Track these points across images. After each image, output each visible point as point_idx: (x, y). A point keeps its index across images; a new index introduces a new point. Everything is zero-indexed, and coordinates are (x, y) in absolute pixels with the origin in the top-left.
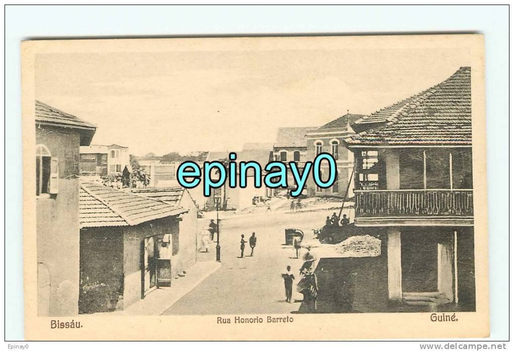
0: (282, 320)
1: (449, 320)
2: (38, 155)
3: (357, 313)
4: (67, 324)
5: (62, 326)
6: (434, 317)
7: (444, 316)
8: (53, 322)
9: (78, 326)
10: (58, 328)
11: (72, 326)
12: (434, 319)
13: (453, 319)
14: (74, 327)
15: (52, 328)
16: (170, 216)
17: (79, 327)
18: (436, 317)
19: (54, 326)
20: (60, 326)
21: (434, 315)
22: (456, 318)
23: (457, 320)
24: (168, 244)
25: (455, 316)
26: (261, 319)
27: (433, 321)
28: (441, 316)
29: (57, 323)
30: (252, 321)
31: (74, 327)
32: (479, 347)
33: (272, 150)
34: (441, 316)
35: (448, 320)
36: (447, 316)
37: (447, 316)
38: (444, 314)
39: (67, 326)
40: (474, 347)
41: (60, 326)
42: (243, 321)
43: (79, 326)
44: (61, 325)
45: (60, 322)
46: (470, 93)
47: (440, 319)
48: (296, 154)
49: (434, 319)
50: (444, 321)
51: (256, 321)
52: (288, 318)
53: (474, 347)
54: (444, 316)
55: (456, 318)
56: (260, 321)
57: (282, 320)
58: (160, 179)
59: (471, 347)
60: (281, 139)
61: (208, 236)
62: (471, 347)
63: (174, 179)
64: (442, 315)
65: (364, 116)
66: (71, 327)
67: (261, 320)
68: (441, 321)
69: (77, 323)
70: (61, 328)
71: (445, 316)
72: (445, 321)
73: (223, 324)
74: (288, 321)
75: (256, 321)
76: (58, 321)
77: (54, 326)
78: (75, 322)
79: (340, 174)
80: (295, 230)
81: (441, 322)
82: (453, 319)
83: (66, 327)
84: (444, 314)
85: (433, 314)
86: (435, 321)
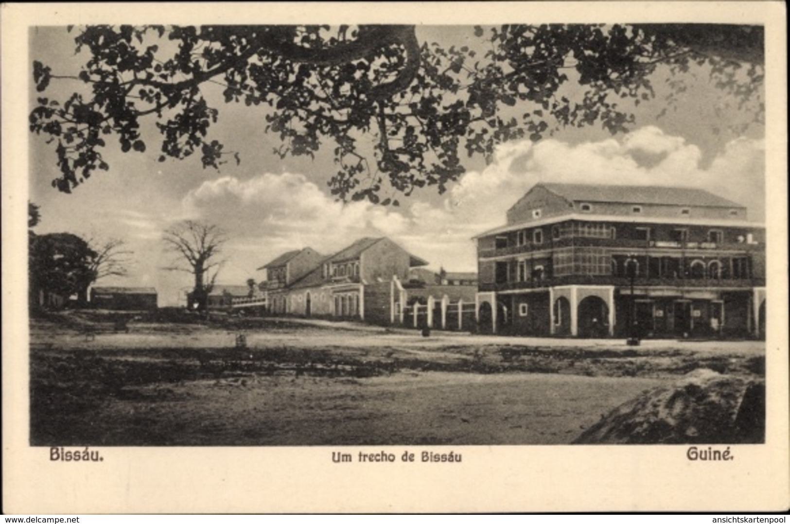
0: (367, 459)
2: (49, 101)
5: (69, 458)
7: (710, 453)
9: (94, 457)
11: (86, 458)
15: (52, 459)
17: (97, 460)
18: (696, 453)
24: (175, 414)
25: (728, 452)
28: (706, 452)
30: (444, 458)
31: (88, 459)
37: (715, 452)
38: (710, 448)
39: (77, 458)
41: (65, 457)
47: (703, 456)
49: (693, 456)
50: (710, 459)
54: (710, 453)
55: (730, 455)
56: (391, 458)
57: (367, 459)
58: (179, 310)
60: (413, 106)
64: (708, 450)
65: (187, 257)
66: (84, 459)
67: (391, 458)
70: (67, 460)
71: (712, 450)
79: (420, 276)
82: (726, 456)
84: (710, 448)
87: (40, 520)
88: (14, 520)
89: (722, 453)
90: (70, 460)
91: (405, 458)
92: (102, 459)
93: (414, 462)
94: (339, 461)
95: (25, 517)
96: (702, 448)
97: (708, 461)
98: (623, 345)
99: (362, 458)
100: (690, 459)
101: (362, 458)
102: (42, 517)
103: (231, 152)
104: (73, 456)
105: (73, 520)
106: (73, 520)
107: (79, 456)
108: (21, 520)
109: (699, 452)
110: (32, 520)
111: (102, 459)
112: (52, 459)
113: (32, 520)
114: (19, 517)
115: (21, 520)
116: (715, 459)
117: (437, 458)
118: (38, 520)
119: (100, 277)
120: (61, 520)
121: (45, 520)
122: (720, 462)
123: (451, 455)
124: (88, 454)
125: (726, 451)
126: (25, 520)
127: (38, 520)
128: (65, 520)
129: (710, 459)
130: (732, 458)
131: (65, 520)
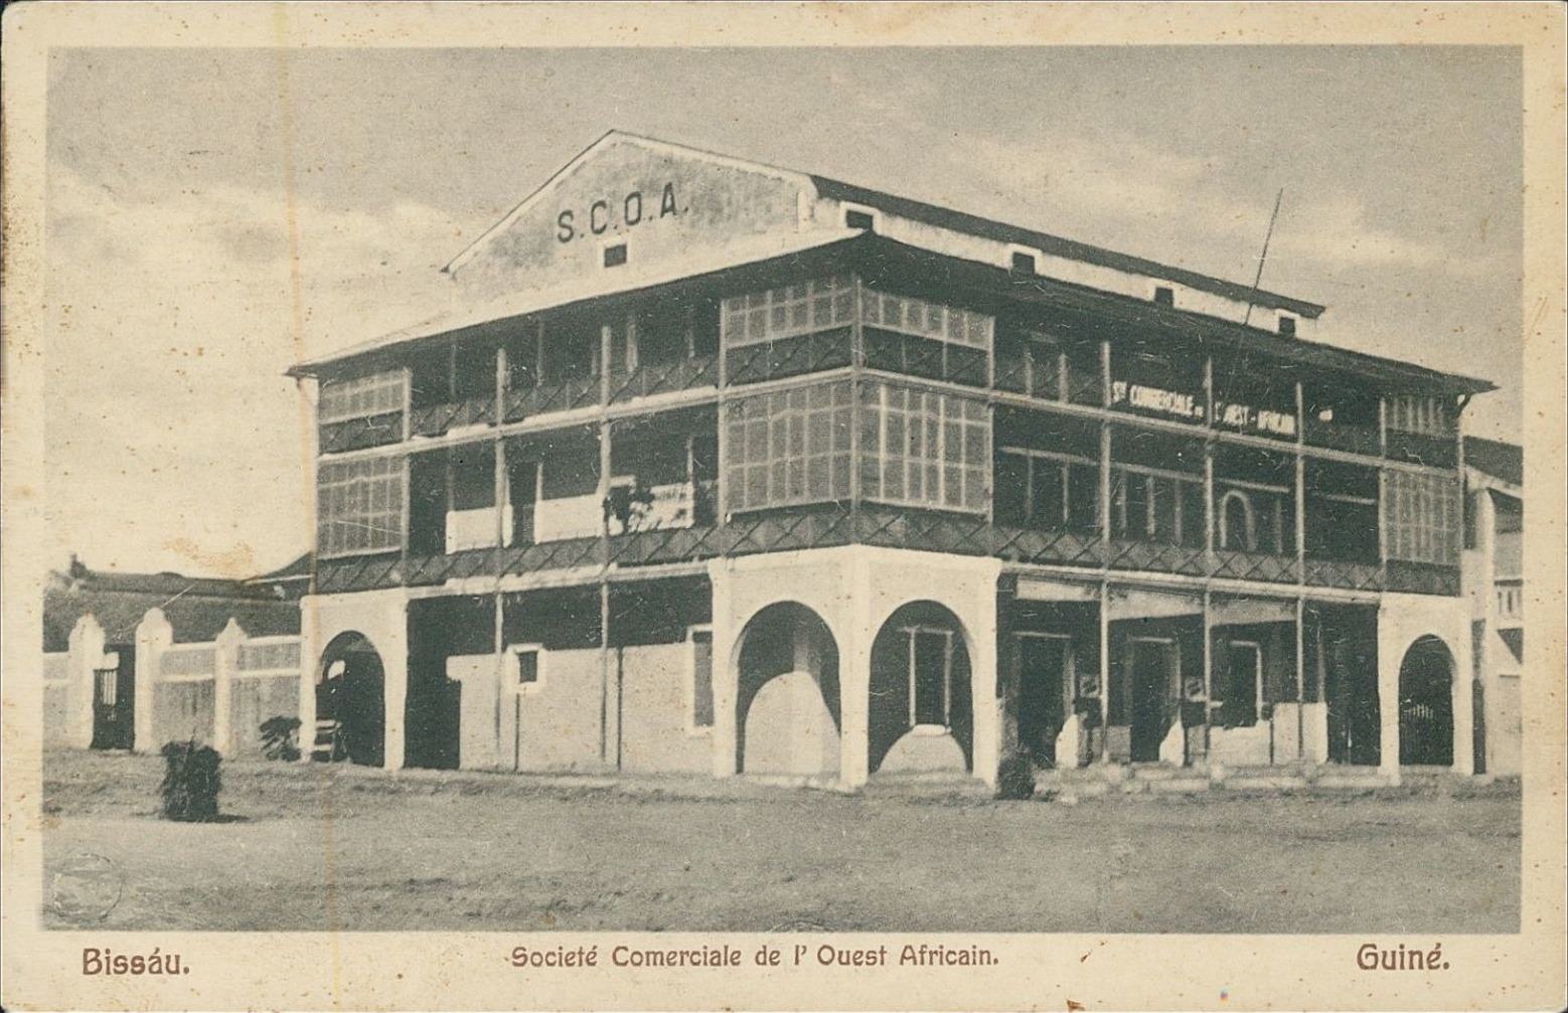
4: (120, 961)
6: (1367, 955)
7: (1402, 954)
8: (92, 955)
9: (173, 967)
10: (108, 973)
11: (964, 960)
14: (967, 963)
15: (86, 972)
16: (772, 605)
17: (177, 972)
18: (1375, 955)
19: (93, 966)
20: (112, 966)
21: (1372, 950)
25: (1439, 954)
26: (534, 954)
27: (1366, 968)
28: (1394, 953)
29: (102, 957)
31: (160, 971)
34: (1394, 953)
35: (658, 962)
39: (137, 969)
41: (112, 966)
43: (172, 966)
47: (1389, 963)
48: (611, 254)
50: (1402, 967)
51: (936, 958)
52: (581, 953)
54: (1402, 954)
55: (1441, 961)
56: (876, 957)
57: (687, 959)
61: (545, 658)
68: (1393, 967)
69: (168, 957)
70: (116, 972)
73: (709, 966)
75: (936, 958)
76: (108, 951)
77: (93, 966)
80: (243, 582)
81: (1391, 972)
83: (133, 972)
85: (1365, 946)
89: (836, 961)
92: (902, 963)
93: (741, 967)
94: (848, 963)
96: (1386, 942)
98: (1028, 576)
99: (927, 956)
100: (1363, 966)
101: (927, 956)
103: (471, 789)
109: (1379, 952)
111: (186, 970)
112: (86, 972)
125: (1432, 953)
129: (1402, 967)
130: (1446, 966)
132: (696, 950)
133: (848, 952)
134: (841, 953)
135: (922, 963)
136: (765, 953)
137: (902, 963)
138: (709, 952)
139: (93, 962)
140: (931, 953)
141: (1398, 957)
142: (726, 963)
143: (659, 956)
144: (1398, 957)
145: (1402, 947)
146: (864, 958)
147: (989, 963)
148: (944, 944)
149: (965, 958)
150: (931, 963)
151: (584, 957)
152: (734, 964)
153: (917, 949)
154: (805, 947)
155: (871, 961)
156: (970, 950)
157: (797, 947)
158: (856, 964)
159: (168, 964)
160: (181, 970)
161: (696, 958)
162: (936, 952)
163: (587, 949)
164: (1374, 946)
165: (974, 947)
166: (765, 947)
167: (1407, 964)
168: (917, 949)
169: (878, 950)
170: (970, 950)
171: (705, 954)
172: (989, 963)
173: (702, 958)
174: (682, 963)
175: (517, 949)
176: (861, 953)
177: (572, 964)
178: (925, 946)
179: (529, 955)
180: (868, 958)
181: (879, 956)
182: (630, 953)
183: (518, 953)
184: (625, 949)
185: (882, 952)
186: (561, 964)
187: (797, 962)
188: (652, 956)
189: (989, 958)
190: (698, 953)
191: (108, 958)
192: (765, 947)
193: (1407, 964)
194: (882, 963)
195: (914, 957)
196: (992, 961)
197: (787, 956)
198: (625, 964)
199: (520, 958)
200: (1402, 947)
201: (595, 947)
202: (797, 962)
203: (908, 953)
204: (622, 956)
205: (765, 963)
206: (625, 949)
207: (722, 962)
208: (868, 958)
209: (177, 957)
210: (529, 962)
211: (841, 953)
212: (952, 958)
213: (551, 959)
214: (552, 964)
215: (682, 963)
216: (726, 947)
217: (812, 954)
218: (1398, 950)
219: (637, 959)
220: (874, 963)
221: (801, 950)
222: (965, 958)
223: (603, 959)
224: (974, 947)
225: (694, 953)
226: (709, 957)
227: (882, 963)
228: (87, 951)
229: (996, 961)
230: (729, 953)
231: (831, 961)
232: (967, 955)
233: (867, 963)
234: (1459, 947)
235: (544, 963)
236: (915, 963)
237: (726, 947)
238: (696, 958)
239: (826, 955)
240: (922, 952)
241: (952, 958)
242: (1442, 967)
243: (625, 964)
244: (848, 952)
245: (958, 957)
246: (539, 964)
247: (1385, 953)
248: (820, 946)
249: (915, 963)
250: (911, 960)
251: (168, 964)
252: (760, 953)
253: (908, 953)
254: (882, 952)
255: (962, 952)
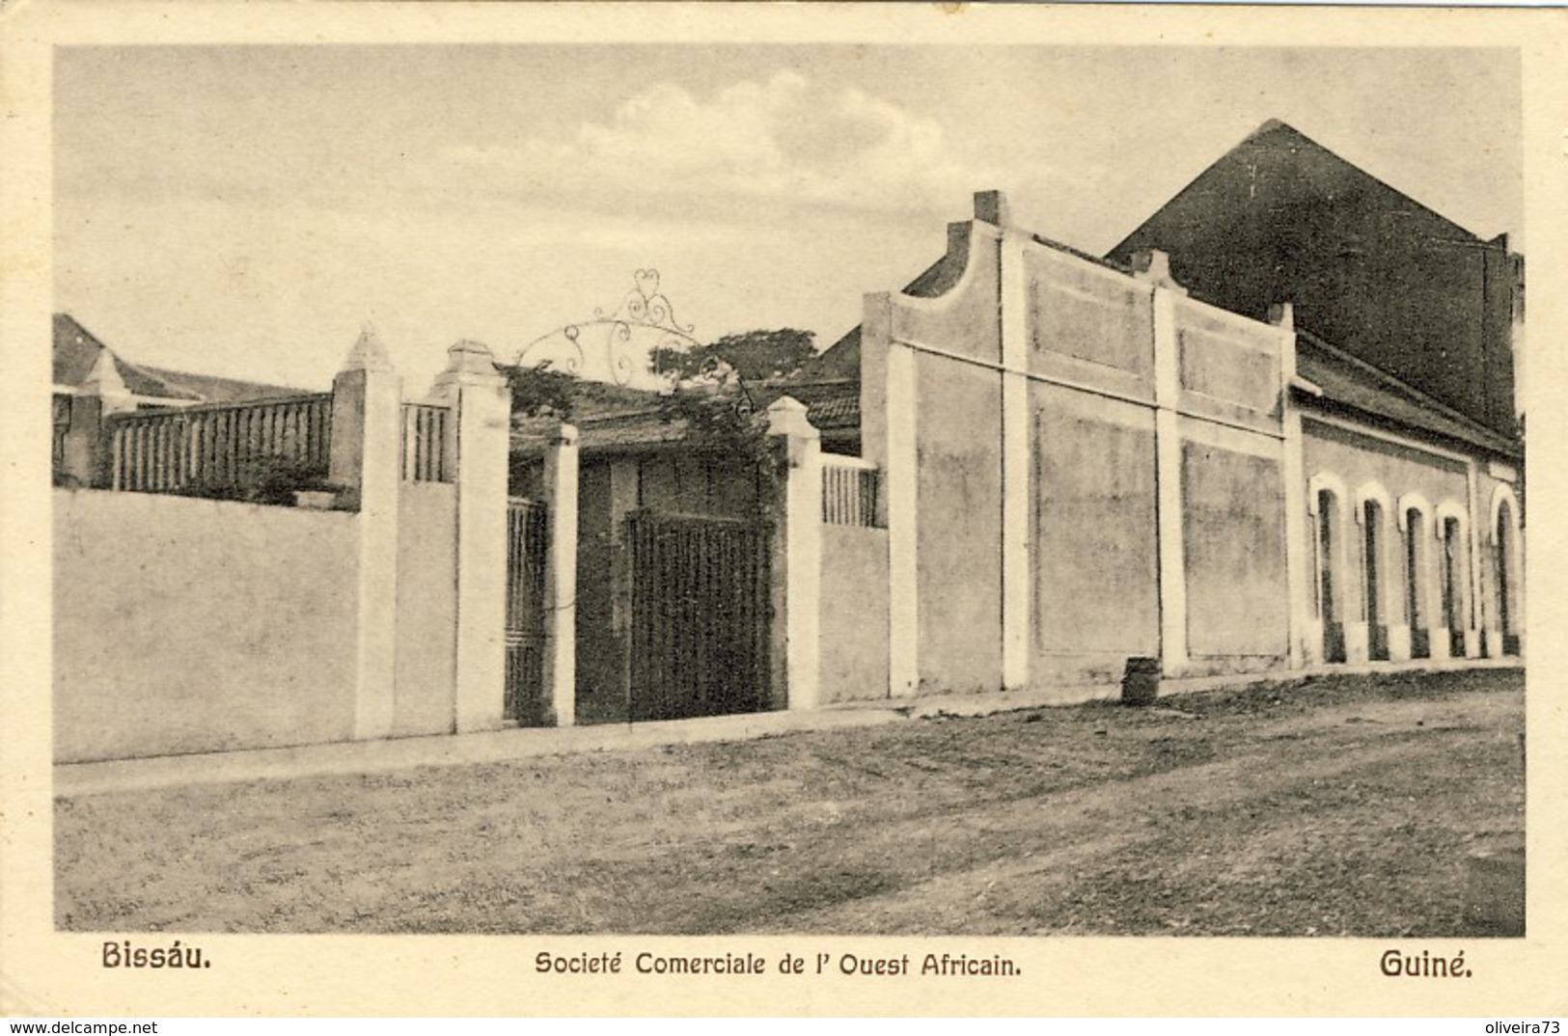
1: (1444, 974)
3: (1490, 934)
6: (1391, 961)
7: (1426, 960)
8: (111, 948)
9: (193, 961)
11: (175, 961)
12: (1393, 968)
13: (1457, 971)
14: (742, 971)
15: (107, 965)
17: (197, 965)
18: (1399, 962)
19: (112, 959)
22: (1465, 968)
23: (1469, 974)
25: (1462, 961)
26: (559, 959)
28: (1417, 959)
29: (121, 951)
30: (157, 959)
31: (179, 965)
32: (113, 1029)
33: (965, 211)
34: (1417, 959)
36: (1004, 963)
40: (103, 1028)
41: (132, 960)
42: (561, 965)
44: (136, 956)
45: (133, 949)
46: (128, 487)
47: (1413, 969)
49: (1393, 968)
50: (1426, 974)
51: (958, 968)
53: (103, 1028)
54: (1426, 960)
55: (1465, 968)
56: (897, 967)
59: (98, 1028)
62: (98, 1028)
63: (430, 395)
66: (171, 965)
68: (1417, 974)
70: (136, 965)
72: (1000, 976)
74: (604, 970)
75: (958, 968)
76: (127, 944)
78: (183, 949)
81: (988, 977)
82: (1455, 968)
83: (154, 966)
85: (1388, 953)
86: (1397, 973)
87: (79, 1029)
88: (28, 1029)
90: (142, 965)
91: (785, 967)
92: (924, 972)
94: (870, 972)
95: (50, 1022)
96: (1411, 948)
97: (746, 974)
99: (949, 966)
101: (949, 966)
102: (84, 1021)
104: (150, 960)
105: (145, 1029)
106: (145, 1029)
107: (163, 959)
108: (42, 1029)
110: (64, 1029)
111: (207, 965)
113: (64, 1029)
114: (38, 1022)
115: (42, 1029)
116: (1004, 973)
117: (138, 959)
118: (75, 1028)
119: (1478, 477)
120: (122, 1029)
121: (89, 1029)
122: (944, 977)
123: (176, 951)
124: (179, 953)
126: (48, 1029)
127: (75, 1028)
128: (130, 1028)
129: (1426, 974)
131: (130, 1028)
132: (720, 957)
133: (870, 962)
134: (863, 962)
135: (944, 972)
136: (789, 961)
137: (924, 972)
138: (732, 959)
139: (111, 957)
140: (953, 963)
141: (1422, 964)
142: (749, 971)
143: (682, 964)
144: (1422, 964)
145: (1426, 953)
146: (886, 968)
147: (1011, 973)
148: (732, 953)
149: (987, 968)
150: (953, 972)
151: (608, 963)
152: (757, 972)
153: (939, 959)
154: (827, 956)
155: (894, 970)
156: (993, 960)
157: (820, 956)
158: (878, 973)
159: (188, 958)
160: (202, 963)
161: (720, 966)
162: (958, 962)
163: (611, 956)
164: (1397, 952)
165: (997, 957)
166: (789, 956)
167: (1000, 970)
168: (939, 959)
169: (901, 959)
170: (993, 960)
171: (729, 962)
172: (1011, 973)
173: (726, 965)
174: (706, 971)
175: (541, 955)
176: (884, 961)
177: (596, 971)
178: (947, 956)
179: (553, 961)
180: (891, 966)
181: (901, 965)
182: (653, 960)
183: (542, 958)
184: (650, 955)
185: (905, 961)
186: (584, 971)
187: (819, 971)
188: (675, 964)
189: (1011, 969)
190: (721, 961)
191: (127, 951)
192: (789, 956)
193: (1000, 970)
194: (904, 972)
195: (936, 967)
196: (1014, 971)
197: (810, 966)
198: (649, 971)
199: (543, 962)
200: (1426, 953)
201: (619, 954)
202: (819, 971)
203: (931, 962)
204: (646, 963)
205: (789, 971)
206: (650, 955)
207: (746, 968)
208: (891, 966)
209: (198, 952)
210: (553, 968)
211: (863, 962)
212: (974, 967)
213: (575, 965)
214: (576, 971)
215: (706, 971)
216: (750, 956)
217: (835, 961)
218: (1422, 957)
219: (661, 965)
220: (896, 972)
221: (823, 958)
222: (987, 968)
223: (628, 964)
224: (997, 957)
225: (718, 960)
226: (733, 965)
227: (904, 972)
228: (106, 944)
229: (1018, 972)
230: (753, 960)
231: (853, 971)
232: (989, 965)
233: (161, 951)
234: (1480, 951)
235: (553, 968)
236: (937, 972)
237: (750, 956)
238: (720, 966)
239: (849, 964)
240: (944, 962)
241: (974, 967)
242: (1465, 974)
243: (649, 971)
244: (870, 962)
245: (980, 967)
246: (563, 971)
247: (1408, 960)
248: (843, 954)
249: (937, 972)
250: (933, 970)
251: (188, 958)
252: (783, 961)
253: (931, 962)
254: (905, 961)
255: (983, 962)
